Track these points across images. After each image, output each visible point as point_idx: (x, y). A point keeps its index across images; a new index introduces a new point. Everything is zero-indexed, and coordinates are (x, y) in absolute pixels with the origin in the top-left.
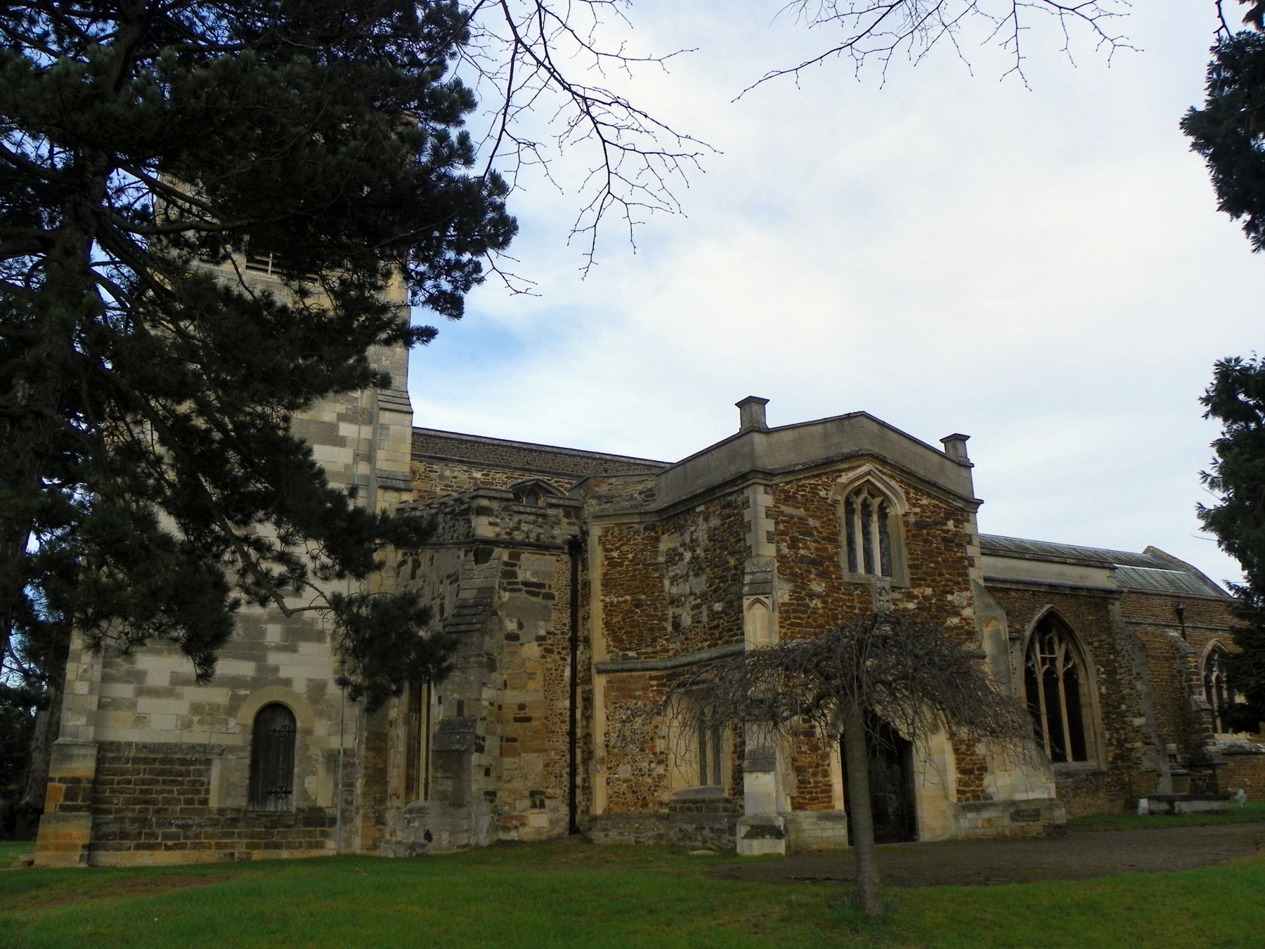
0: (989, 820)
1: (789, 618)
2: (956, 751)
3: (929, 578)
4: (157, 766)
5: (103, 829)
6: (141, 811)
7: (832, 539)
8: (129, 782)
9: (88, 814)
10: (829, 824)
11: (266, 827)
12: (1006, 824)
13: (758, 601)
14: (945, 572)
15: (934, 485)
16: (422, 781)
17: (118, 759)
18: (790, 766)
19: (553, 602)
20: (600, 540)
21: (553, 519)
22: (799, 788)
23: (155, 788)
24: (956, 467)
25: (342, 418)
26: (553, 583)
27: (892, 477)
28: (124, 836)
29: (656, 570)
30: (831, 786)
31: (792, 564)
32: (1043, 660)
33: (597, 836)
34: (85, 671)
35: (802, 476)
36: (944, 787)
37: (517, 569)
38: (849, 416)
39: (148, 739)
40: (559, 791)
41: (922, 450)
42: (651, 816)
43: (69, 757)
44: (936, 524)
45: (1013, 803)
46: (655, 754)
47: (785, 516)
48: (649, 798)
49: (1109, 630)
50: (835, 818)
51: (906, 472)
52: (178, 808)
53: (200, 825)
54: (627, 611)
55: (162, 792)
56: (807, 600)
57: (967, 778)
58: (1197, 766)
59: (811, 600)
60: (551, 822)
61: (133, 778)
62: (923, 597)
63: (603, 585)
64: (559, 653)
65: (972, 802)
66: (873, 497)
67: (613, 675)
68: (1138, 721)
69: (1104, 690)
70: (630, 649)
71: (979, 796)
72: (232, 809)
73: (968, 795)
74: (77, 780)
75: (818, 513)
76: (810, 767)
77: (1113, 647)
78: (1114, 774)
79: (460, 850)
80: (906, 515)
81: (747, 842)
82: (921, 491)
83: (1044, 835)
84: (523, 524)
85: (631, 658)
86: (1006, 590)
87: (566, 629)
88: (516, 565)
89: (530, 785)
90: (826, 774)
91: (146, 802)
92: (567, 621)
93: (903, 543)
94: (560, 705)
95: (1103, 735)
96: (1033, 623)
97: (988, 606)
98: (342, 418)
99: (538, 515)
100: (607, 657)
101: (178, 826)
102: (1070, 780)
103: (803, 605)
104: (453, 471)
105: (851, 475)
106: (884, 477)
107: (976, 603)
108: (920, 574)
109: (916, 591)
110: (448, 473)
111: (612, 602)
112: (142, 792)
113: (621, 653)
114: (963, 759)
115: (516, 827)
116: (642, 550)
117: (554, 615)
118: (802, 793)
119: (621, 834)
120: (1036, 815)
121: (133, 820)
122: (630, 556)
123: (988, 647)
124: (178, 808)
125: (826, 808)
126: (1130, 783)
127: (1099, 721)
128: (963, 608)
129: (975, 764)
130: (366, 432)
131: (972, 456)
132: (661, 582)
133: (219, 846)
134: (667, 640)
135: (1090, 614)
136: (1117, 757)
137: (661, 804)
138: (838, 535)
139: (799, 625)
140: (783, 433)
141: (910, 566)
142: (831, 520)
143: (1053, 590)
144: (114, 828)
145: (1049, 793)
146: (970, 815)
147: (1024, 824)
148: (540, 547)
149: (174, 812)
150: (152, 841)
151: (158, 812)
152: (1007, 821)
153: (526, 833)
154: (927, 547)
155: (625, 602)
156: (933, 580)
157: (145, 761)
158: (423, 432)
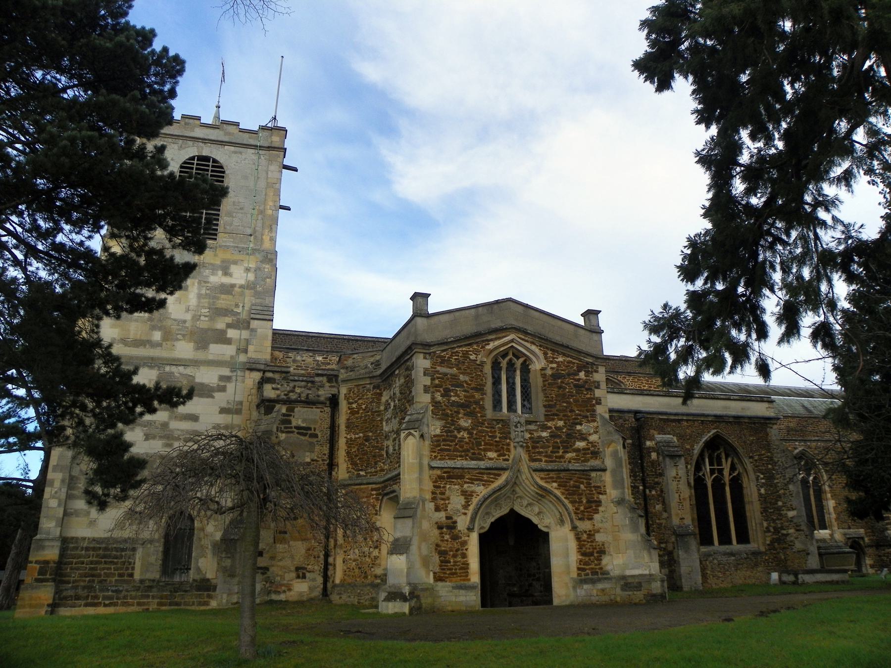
0: (603, 590)
1: (439, 445)
2: (578, 539)
3: (562, 414)
4: (101, 552)
5: (64, 594)
6: (89, 581)
7: (480, 389)
8: (83, 563)
9: (53, 583)
10: (462, 592)
11: (171, 591)
12: (618, 594)
13: (410, 434)
14: (575, 409)
15: (567, 347)
17: (76, 548)
18: (434, 550)
19: (316, 439)
20: (345, 397)
21: (319, 384)
22: (440, 566)
23: (99, 566)
25: (229, 326)
26: (317, 427)
27: (533, 343)
28: (78, 598)
29: (378, 415)
30: (468, 564)
32: (712, 472)
33: (335, 598)
34: (56, 492)
35: (455, 346)
36: (568, 567)
37: (291, 418)
38: (497, 302)
39: (96, 535)
40: (317, 567)
41: (560, 323)
42: (369, 585)
43: (43, 548)
44: (569, 375)
45: (624, 577)
46: (373, 542)
47: (440, 374)
48: (369, 572)
49: (768, 447)
50: (472, 588)
52: (113, 579)
53: (127, 591)
55: (104, 569)
56: (456, 433)
57: (587, 559)
58: (881, 546)
59: (459, 432)
60: (310, 588)
61: (85, 560)
63: (347, 427)
65: (590, 576)
66: (518, 358)
68: (791, 514)
69: (763, 491)
70: (361, 470)
71: (597, 572)
72: (150, 580)
73: (587, 571)
74: (47, 562)
75: (469, 371)
76: (451, 551)
77: (771, 459)
78: (771, 553)
79: (233, 606)
80: (543, 369)
81: (384, 604)
82: (557, 352)
83: (644, 601)
84: (297, 388)
85: (361, 476)
86: (679, 421)
87: (325, 457)
88: (291, 415)
89: (296, 563)
90: (464, 556)
91: (93, 576)
92: (327, 452)
95: (761, 524)
96: (701, 443)
97: (609, 433)
98: (229, 326)
99: (308, 382)
100: (347, 476)
101: (113, 591)
102: (733, 558)
103: (451, 436)
104: (303, 357)
105: (497, 343)
107: (601, 430)
108: (554, 411)
109: (549, 424)
110: (299, 358)
111: (351, 438)
112: (91, 569)
113: (356, 473)
115: (284, 592)
116: (371, 402)
117: (317, 448)
118: (444, 569)
119: (349, 596)
120: (639, 586)
121: (84, 588)
122: (363, 407)
123: (609, 463)
124: (113, 579)
125: (464, 580)
126: (786, 560)
127: (758, 514)
130: (245, 334)
131: (602, 325)
132: (382, 423)
133: (139, 604)
134: (383, 463)
135: (750, 435)
136: (772, 542)
137: (376, 577)
138: (485, 386)
139: (449, 450)
140: (441, 317)
141: (545, 406)
142: (480, 375)
143: (719, 419)
144: (70, 593)
145: (650, 570)
146: (585, 587)
147: (630, 593)
148: (309, 403)
149: (111, 581)
150: (96, 601)
151: (101, 582)
152: (618, 591)
153: (292, 596)
154: (560, 392)
155: (359, 438)
156: (564, 416)
157: (94, 549)
158: (282, 332)
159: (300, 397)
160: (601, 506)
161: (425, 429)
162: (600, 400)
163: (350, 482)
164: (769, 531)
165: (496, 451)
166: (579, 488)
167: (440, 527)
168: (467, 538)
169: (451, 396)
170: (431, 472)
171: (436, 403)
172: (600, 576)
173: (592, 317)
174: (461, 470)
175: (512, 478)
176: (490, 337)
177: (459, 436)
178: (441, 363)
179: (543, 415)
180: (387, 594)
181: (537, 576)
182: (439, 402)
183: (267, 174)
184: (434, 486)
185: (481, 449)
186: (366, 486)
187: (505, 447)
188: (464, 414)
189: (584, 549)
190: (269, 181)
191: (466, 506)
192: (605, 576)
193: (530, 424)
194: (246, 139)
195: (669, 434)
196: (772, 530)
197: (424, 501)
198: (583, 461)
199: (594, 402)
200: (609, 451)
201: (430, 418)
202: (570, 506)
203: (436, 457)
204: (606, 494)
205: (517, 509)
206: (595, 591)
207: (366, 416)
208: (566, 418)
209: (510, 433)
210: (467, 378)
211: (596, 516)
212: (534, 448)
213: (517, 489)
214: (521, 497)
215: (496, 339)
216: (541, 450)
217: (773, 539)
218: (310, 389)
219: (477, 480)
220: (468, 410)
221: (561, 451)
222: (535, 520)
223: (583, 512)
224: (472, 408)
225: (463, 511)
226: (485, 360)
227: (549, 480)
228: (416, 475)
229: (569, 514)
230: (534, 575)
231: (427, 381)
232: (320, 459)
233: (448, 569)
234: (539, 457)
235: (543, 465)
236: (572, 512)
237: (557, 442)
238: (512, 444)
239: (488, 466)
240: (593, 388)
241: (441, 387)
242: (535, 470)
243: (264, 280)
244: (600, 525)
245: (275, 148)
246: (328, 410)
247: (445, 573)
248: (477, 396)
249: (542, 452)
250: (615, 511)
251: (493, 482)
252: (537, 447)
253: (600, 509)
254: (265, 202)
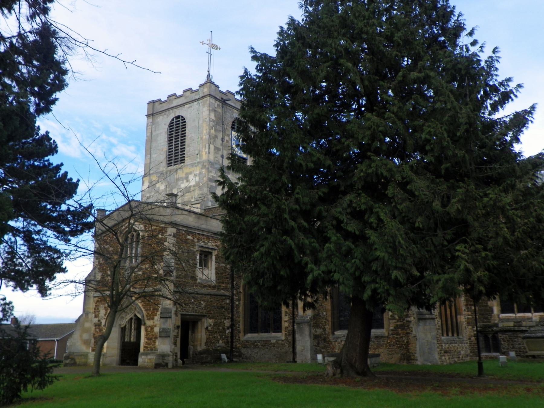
0: (150, 359)
16: (133, 331)
71: (153, 349)
78: (393, 338)
129: (153, 336)
136: (396, 327)
164: (394, 319)
167: (96, 326)
196: (397, 318)
206: (146, 360)
217: (397, 325)
223: (150, 315)
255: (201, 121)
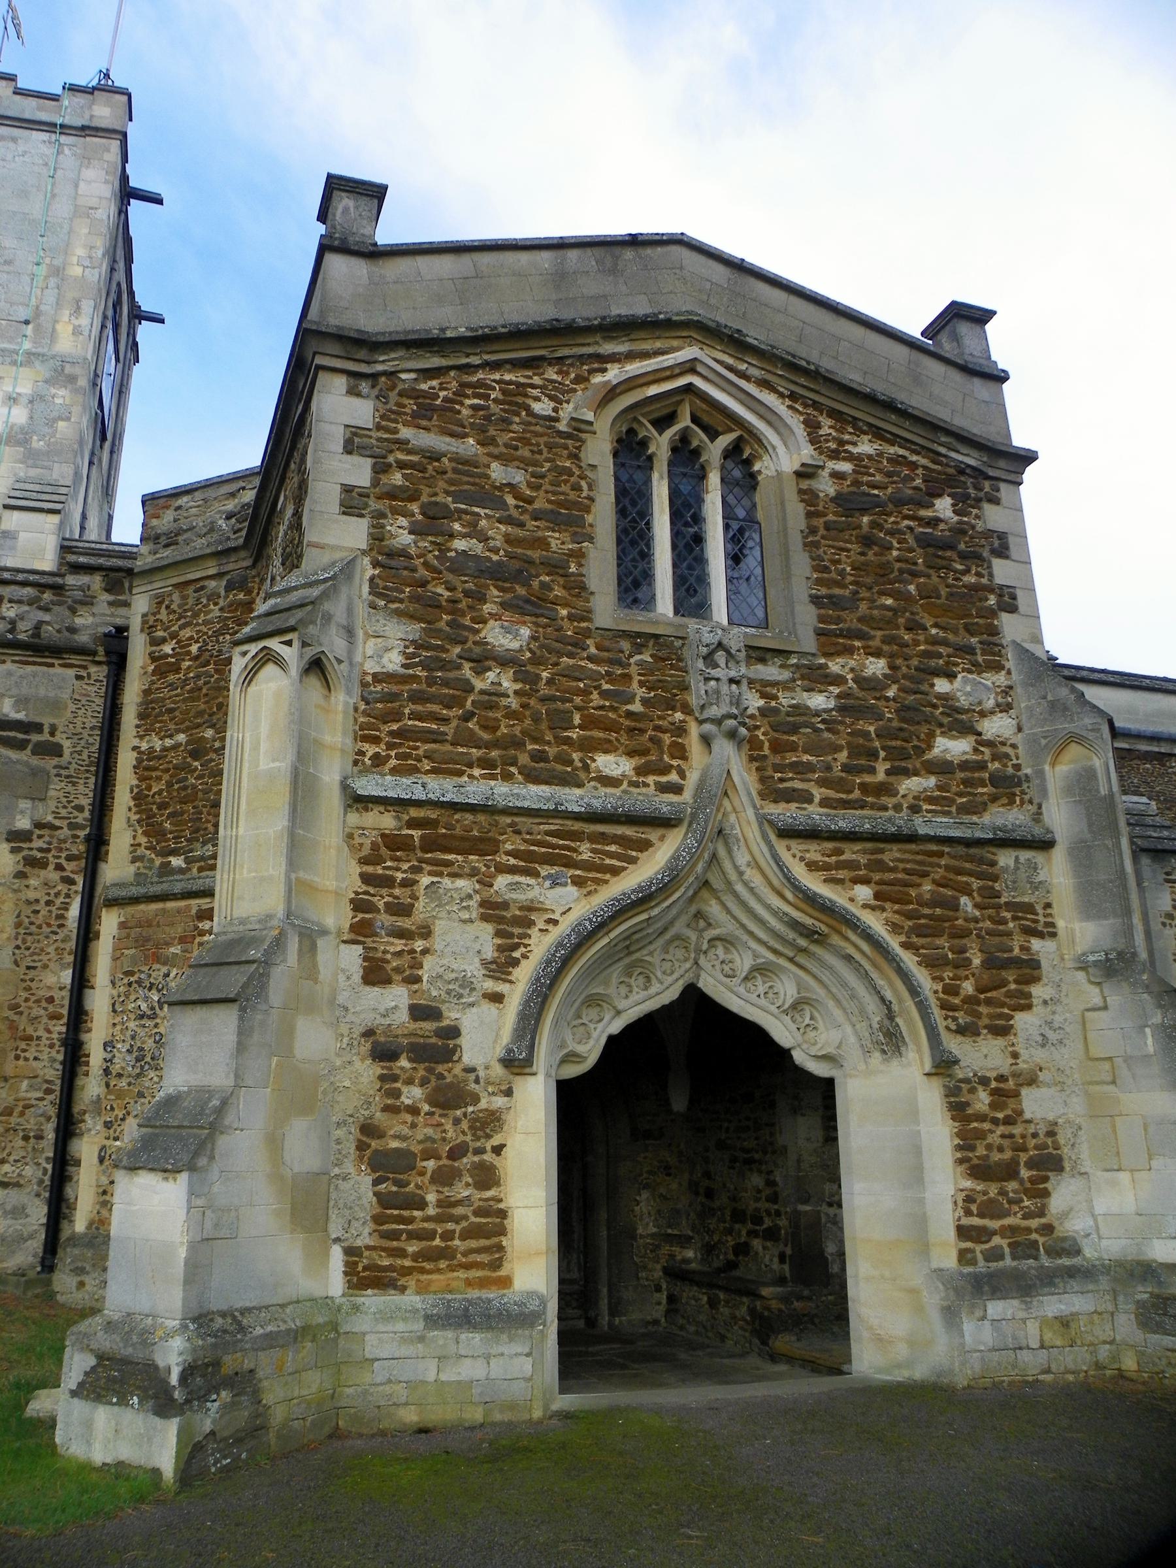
0: (1064, 1322)
1: (397, 716)
2: (958, 1110)
10: (473, 1340)
13: (268, 657)
14: (928, 621)
15: (889, 406)
18: (350, 1147)
19: (55, 761)
20: (144, 622)
22: (378, 1219)
24: (956, 376)
26: (60, 722)
27: (764, 384)
30: (503, 1214)
31: (423, 572)
35: (475, 360)
36: (920, 1223)
38: (634, 241)
44: (899, 502)
47: (409, 452)
51: (805, 372)
54: (176, 767)
56: (467, 671)
57: (993, 1190)
59: (480, 672)
62: (859, 680)
64: (59, 867)
65: (1008, 1262)
66: (713, 435)
67: (130, 910)
70: (174, 852)
73: (997, 1240)
75: (525, 452)
80: (805, 473)
81: (79, 1407)
87: (83, 817)
90: (487, 1177)
93: (796, 540)
94: (50, 979)
103: (446, 683)
105: (634, 368)
106: (742, 383)
107: (1022, 700)
108: (851, 621)
111: (151, 749)
113: (158, 861)
114: (981, 1135)
117: (56, 789)
118: (394, 1236)
122: (194, 648)
125: (483, 1283)
128: (983, 714)
141: (815, 600)
146: (995, 1308)
152: (1126, 1326)
156: (887, 640)
159: (12, 630)
160: (1036, 979)
161: (333, 644)
162: (1014, 597)
163: (135, 891)
165: (630, 754)
166: (956, 907)
167: (384, 1053)
168: (499, 1102)
169: (452, 536)
170: (354, 818)
171: (390, 555)
172: (1046, 1261)
173: (964, 329)
174: (481, 818)
175: (694, 857)
176: (608, 348)
177: (479, 685)
178: (415, 415)
179: (812, 633)
180: (93, 1361)
181: (768, 1223)
182: (403, 553)
183: (77, 186)
184: (366, 878)
185: (568, 741)
186: (182, 904)
187: (667, 739)
188: (504, 605)
189: (981, 1151)
190: (81, 201)
191: (501, 967)
192: (1065, 1261)
193: (762, 660)
194: (29, 108)
195: (1136, 793)
197: (310, 937)
198: (964, 810)
199: (992, 600)
200: (1057, 774)
201: (361, 610)
202: (923, 977)
203: (378, 760)
204: (1053, 935)
205: (714, 986)
206: (1033, 1328)
207: (198, 677)
208: (894, 651)
209: (685, 688)
210: (519, 477)
211: (1021, 1020)
212: (777, 747)
213: (714, 909)
214: (727, 941)
215: (631, 356)
216: (806, 758)
218: (46, 609)
219: (549, 860)
220: (521, 591)
221: (882, 767)
222: (782, 1032)
223: (969, 1000)
224: (535, 584)
225: (490, 985)
226: (589, 416)
227: (841, 874)
228: (279, 823)
229: (922, 1007)
230: (757, 1220)
231: (360, 472)
232: (64, 823)
233: (413, 1236)
234: (797, 785)
235: (815, 814)
236: (933, 1002)
237: (866, 735)
238: (694, 730)
239: (597, 804)
240: (986, 554)
241: (413, 498)
242: (787, 833)
243: (52, 422)
244: (1039, 1056)
245: (97, 129)
246: (99, 672)
247: (401, 1253)
248: (558, 542)
249: (810, 768)
250: (1097, 1000)
251: (615, 871)
252: (793, 748)
253: (1038, 991)
254: (67, 250)
255: (62, 209)
